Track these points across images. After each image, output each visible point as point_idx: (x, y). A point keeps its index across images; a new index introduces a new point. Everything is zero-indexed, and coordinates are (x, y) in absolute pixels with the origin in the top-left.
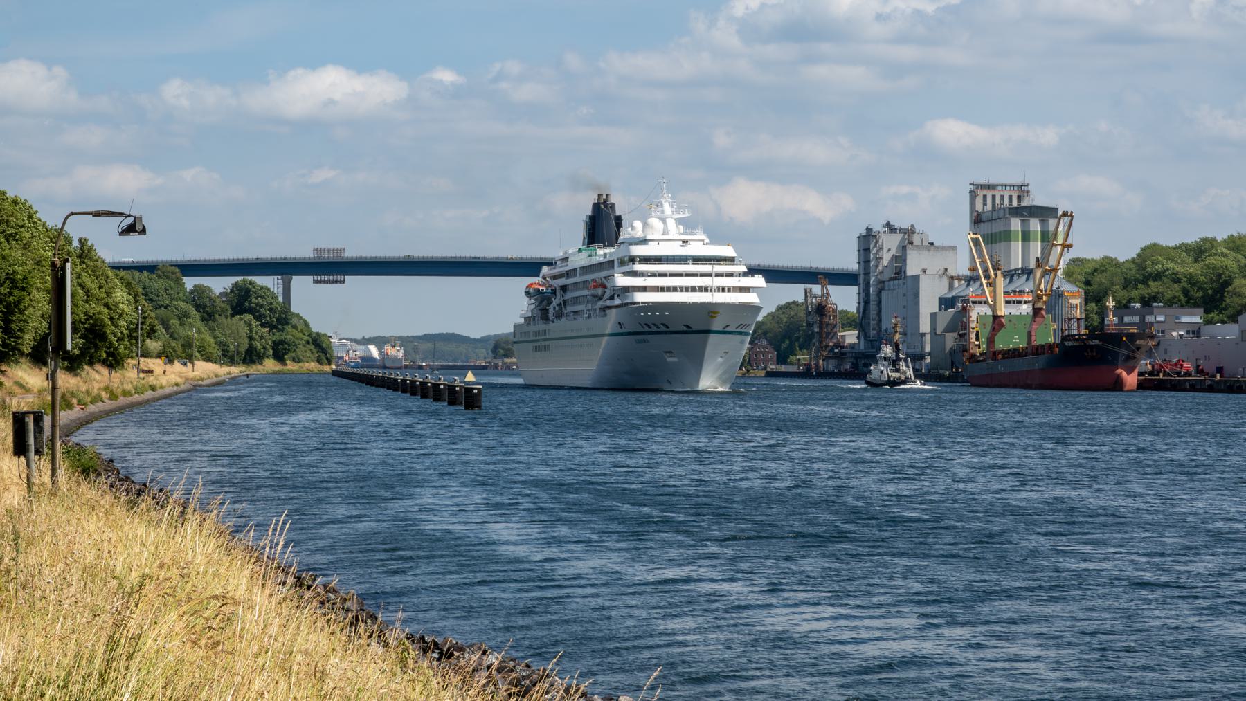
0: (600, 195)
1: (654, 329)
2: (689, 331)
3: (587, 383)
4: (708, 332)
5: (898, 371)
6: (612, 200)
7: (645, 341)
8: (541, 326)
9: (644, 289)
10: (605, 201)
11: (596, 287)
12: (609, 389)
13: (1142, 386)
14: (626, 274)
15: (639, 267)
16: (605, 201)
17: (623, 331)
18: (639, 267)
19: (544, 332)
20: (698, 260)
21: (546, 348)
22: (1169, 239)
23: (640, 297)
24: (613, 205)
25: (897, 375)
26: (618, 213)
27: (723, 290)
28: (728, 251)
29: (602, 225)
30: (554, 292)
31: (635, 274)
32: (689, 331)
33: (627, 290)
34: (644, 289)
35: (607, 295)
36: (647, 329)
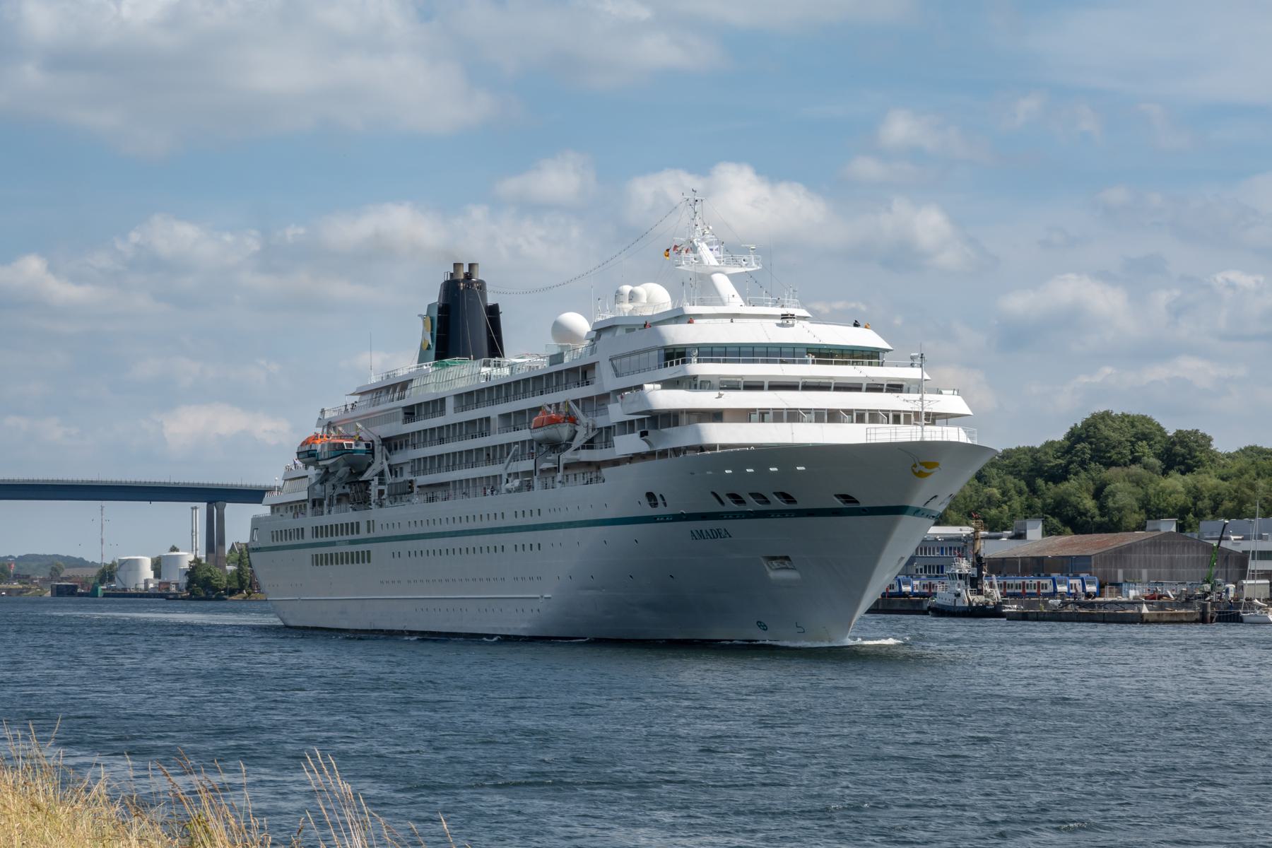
0: (457, 266)
1: (752, 505)
2: (850, 507)
3: (520, 625)
4: (900, 510)
5: (980, 592)
6: (479, 275)
7: (717, 534)
8: (343, 515)
9: (716, 416)
10: (468, 277)
11: (553, 422)
12: (600, 642)
13: (106, 595)
14: (669, 384)
15: (697, 368)
16: (468, 277)
17: (660, 510)
18: (697, 368)
19: (355, 527)
20: (824, 354)
21: (365, 557)
22: (1117, 411)
23: (717, 434)
24: (482, 285)
25: (981, 599)
26: (490, 301)
27: (897, 420)
28: (866, 338)
29: (461, 321)
30: (370, 449)
31: (693, 383)
32: (850, 507)
33: (671, 418)
34: (716, 416)
35: (580, 439)
36: (731, 506)
